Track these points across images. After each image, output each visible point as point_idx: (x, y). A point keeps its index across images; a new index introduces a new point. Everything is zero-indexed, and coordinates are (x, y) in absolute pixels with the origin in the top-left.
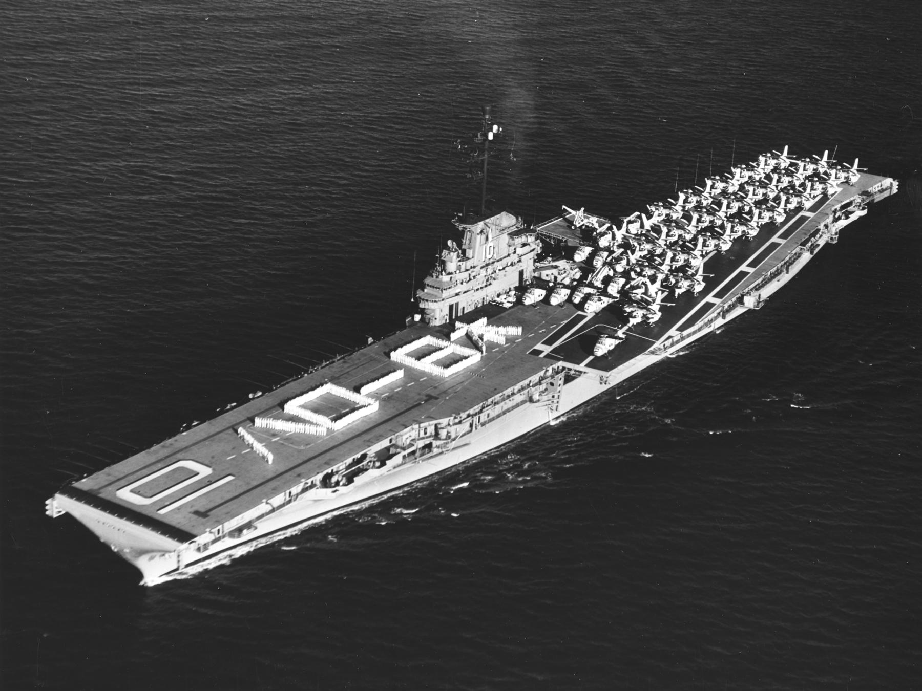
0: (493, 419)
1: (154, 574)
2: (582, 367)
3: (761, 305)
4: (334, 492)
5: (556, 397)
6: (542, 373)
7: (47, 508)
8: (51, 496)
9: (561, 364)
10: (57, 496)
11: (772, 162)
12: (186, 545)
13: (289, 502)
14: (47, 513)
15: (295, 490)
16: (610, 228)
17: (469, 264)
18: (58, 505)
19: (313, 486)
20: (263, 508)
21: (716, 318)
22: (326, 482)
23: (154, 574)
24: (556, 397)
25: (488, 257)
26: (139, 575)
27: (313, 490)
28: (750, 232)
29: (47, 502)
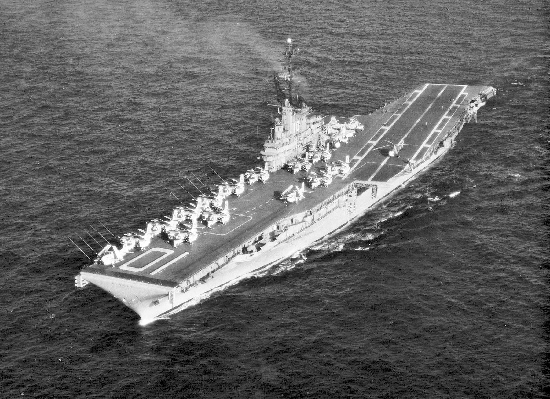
0: (322, 217)
1: (147, 317)
2: (369, 182)
3: (454, 146)
4: (251, 256)
5: (353, 204)
6: (320, 204)
7: (76, 281)
8: (78, 273)
9: (356, 182)
10: (82, 273)
11: (229, 190)
12: (175, 288)
13: (227, 263)
14: (76, 285)
15: (230, 255)
16: (111, 249)
17: (288, 133)
18: (83, 279)
19: (238, 253)
20: (214, 266)
21: (431, 155)
22: (245, 250)
23: (147, 317)
24: (353, 204)
25: (298, 130)
26: (137, 317)
27: (238, 256)
28: (325, 181)
29: (76, 278)
